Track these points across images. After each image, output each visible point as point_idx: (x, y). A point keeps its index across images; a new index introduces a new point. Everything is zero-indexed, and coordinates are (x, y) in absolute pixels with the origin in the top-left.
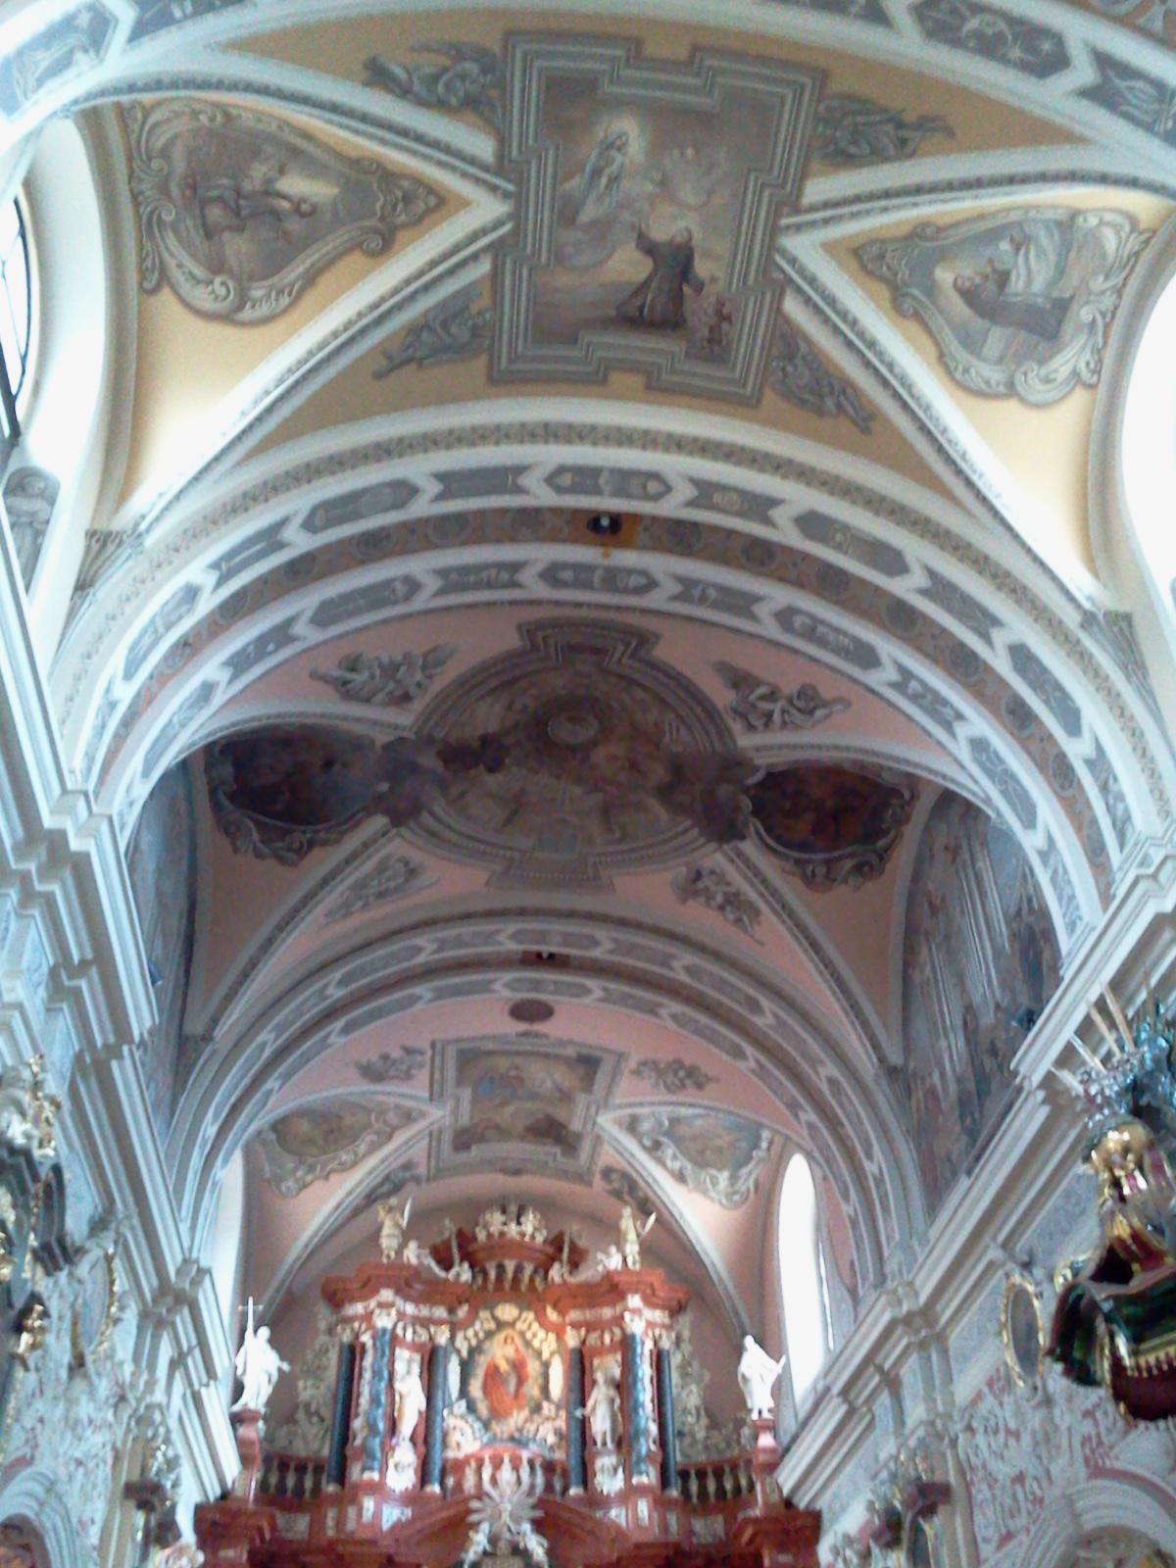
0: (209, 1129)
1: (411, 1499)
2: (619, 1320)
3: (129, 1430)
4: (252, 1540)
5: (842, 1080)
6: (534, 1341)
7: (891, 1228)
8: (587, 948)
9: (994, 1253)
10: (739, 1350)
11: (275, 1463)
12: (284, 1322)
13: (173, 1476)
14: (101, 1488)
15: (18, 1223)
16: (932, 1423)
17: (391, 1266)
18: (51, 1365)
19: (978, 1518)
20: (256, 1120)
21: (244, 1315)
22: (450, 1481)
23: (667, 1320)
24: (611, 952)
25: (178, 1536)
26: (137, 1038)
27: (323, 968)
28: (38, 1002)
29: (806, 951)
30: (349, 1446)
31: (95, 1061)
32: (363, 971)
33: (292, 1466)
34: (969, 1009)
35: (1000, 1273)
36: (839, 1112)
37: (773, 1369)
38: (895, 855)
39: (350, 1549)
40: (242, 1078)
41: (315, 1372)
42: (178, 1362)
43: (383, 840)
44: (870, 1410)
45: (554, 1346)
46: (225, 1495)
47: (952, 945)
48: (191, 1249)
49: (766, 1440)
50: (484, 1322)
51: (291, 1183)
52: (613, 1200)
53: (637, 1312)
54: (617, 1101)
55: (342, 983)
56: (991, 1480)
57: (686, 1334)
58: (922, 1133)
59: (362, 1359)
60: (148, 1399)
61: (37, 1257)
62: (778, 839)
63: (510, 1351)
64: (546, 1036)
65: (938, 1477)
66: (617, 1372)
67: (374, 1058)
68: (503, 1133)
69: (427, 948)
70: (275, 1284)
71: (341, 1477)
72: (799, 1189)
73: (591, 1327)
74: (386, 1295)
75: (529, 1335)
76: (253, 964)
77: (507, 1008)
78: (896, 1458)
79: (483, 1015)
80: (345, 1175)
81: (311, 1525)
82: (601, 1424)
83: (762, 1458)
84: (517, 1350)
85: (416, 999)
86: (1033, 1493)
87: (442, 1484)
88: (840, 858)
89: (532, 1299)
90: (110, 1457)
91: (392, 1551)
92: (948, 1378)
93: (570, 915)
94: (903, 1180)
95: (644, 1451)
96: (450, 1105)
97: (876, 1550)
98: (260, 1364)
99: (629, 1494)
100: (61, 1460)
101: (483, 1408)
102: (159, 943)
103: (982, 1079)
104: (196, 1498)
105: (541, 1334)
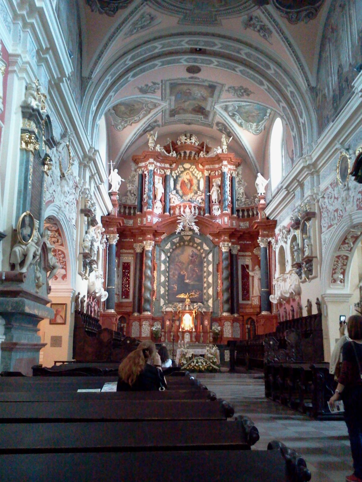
0: (94, 108)
1: (160, 216)
2: (220, 168)
3: (80, 195)
4: (118, 226)
5: (295, 91)
6: (195, 174)
7: (306, 139)
8: (212, 46)
9: (338, 146)
10: (256, 177)
11: (122, 207)
12: (122, 168)
13: (94, 208)
14: (74, 210)
15: (38, 132)
16: (312, 196)
17: (152, 152)
18: (55, 176)
19: (323, 221)
20: (108, 106)
21: (110, 166)
22: (172, 212)
23: (235, 168)
24: (220, 48)
25: (97, 223)
26: (67, 76)
27: (125, 54)
28: (34, 62)
29: (287, 47)
30: (143, 202)
31: (55, 83)
32: (138, 55)
33: (127, 207)
34: (340, 66)
35: (339, 152)
36: (293, 102)
37: (266, 182)
38: (322, 9)
39: (145, 228)
40: (102, 91)
41: (132, 182)
42: (92, 177)
43: (142, 6)
44: (294, 193)
45: (201, 175)
46: (109, 214)
47: (337, 43)
48: (92, 145)
49: (262, 201)
50: (180, 168)
51: (120, 126)
52: (219, 132)
53: (226, 166)
54: (222, 100)
55: (131, 59)
56: (328, 211)
57: (240, 172)
58: (319, 109)
59: (145, 178)
60: (84, 187)
61: (46, 144)
62: (280, 4)
63: (188, 177)
64: (199, 79)
65: (312, 211)
66: (219, 183)
67: (143, 86)
68: (185, 111)
69: (158, 47)
70: (118, 157)
71: (141, 210)
72: (278, 128)
73: (212, 170)
74: (151, 160)
75: (194, 172)
76: (102, 53)
77: (186, 69)
78: (300, 206)
79: (177, 71)
80: (138, 123)
81: (134, 222)
82: (214, 197)
83: (261, 206)
84: (190, 177)
85: (155, 65)
86: (340, 214)
87: (169, 212)
88: (303, 11)
89: (194, 162)
90: (75, 202)
91: (156, 229)
92: (319, 183)
93: (206, 34)
94: (311, 124)
95: (227, 204)
96: (168, 102)
97: (292, 230)
98: (116, 179)
99: (222, 215)
100: (62, 202)
101: (180, 192)
102: (71, 44)
103: (341, 90)
104: (102, 215)
105: (197, 172)
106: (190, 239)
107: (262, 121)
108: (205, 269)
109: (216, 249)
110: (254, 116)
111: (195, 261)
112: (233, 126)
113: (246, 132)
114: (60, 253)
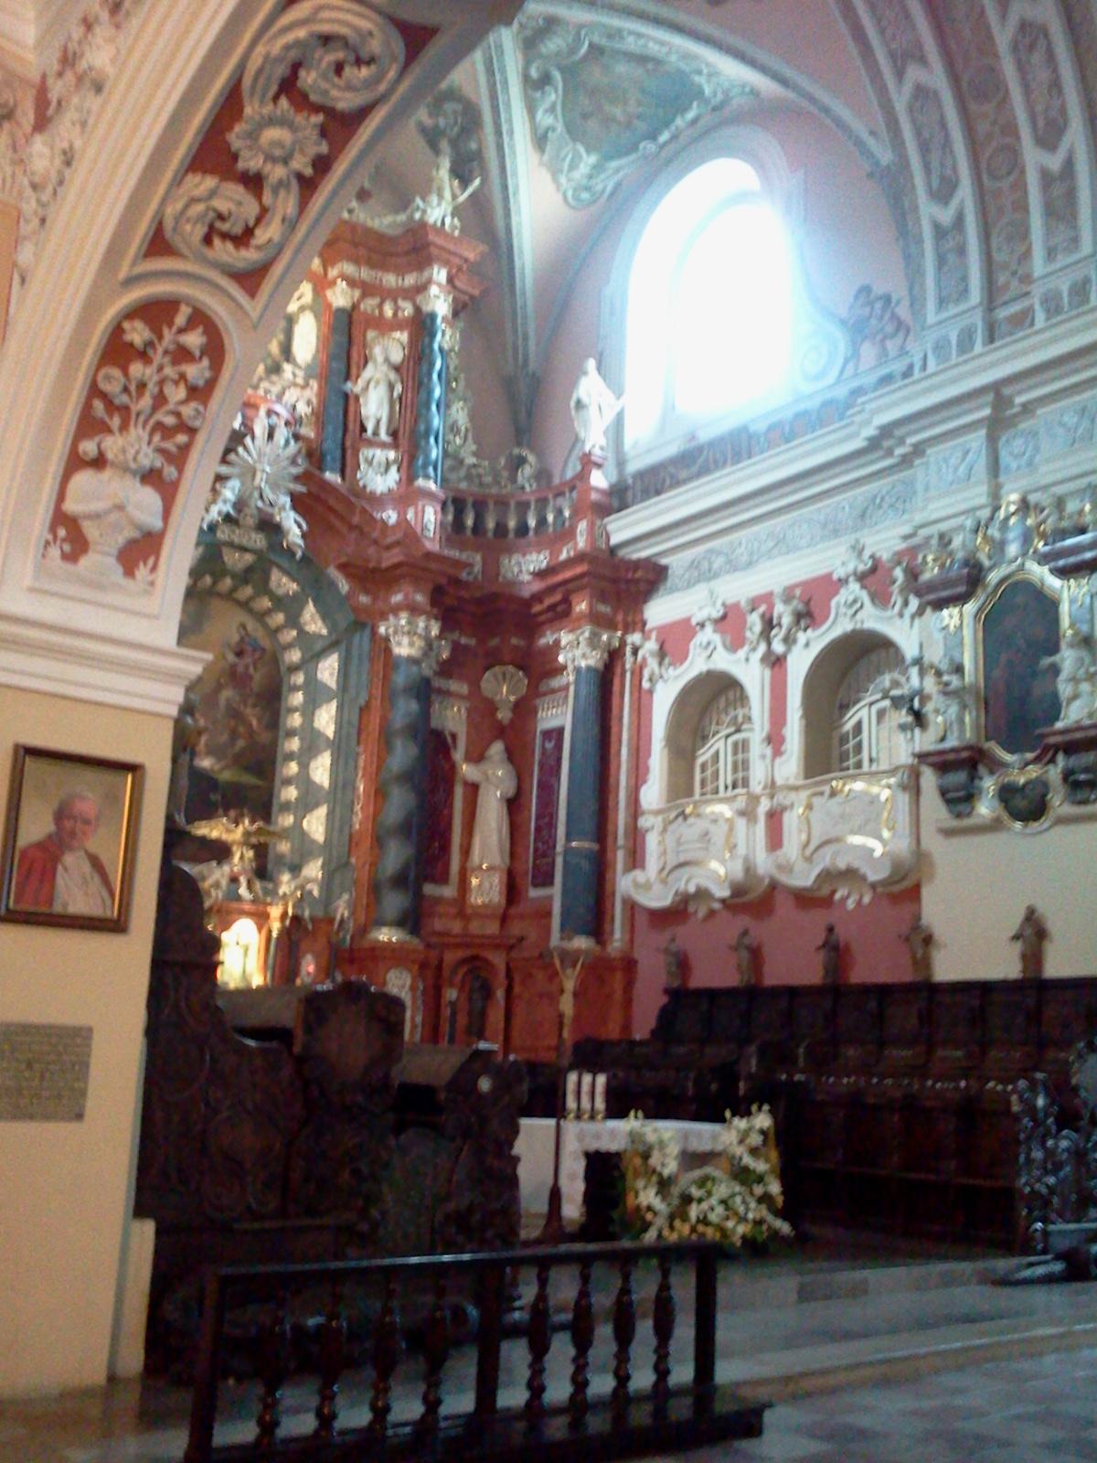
37: (611, 406)
82: (375, 406)
106: (249, 570)
107: (627, 153)
108: (296, 720)
109: (361, 641)
110: (614, 119)
111: (251, 677)
112: (511, 133)
113: (545, 176)
114: (194, 340)
